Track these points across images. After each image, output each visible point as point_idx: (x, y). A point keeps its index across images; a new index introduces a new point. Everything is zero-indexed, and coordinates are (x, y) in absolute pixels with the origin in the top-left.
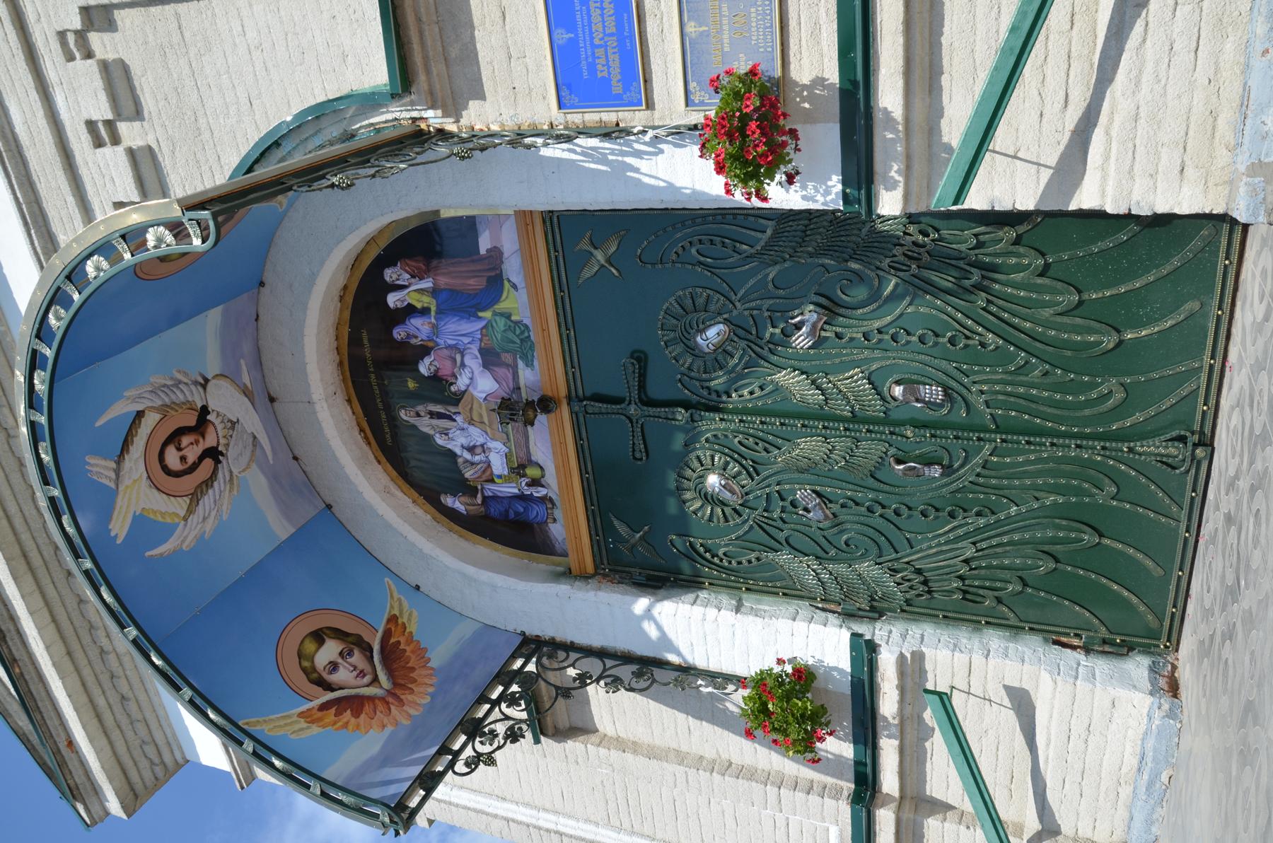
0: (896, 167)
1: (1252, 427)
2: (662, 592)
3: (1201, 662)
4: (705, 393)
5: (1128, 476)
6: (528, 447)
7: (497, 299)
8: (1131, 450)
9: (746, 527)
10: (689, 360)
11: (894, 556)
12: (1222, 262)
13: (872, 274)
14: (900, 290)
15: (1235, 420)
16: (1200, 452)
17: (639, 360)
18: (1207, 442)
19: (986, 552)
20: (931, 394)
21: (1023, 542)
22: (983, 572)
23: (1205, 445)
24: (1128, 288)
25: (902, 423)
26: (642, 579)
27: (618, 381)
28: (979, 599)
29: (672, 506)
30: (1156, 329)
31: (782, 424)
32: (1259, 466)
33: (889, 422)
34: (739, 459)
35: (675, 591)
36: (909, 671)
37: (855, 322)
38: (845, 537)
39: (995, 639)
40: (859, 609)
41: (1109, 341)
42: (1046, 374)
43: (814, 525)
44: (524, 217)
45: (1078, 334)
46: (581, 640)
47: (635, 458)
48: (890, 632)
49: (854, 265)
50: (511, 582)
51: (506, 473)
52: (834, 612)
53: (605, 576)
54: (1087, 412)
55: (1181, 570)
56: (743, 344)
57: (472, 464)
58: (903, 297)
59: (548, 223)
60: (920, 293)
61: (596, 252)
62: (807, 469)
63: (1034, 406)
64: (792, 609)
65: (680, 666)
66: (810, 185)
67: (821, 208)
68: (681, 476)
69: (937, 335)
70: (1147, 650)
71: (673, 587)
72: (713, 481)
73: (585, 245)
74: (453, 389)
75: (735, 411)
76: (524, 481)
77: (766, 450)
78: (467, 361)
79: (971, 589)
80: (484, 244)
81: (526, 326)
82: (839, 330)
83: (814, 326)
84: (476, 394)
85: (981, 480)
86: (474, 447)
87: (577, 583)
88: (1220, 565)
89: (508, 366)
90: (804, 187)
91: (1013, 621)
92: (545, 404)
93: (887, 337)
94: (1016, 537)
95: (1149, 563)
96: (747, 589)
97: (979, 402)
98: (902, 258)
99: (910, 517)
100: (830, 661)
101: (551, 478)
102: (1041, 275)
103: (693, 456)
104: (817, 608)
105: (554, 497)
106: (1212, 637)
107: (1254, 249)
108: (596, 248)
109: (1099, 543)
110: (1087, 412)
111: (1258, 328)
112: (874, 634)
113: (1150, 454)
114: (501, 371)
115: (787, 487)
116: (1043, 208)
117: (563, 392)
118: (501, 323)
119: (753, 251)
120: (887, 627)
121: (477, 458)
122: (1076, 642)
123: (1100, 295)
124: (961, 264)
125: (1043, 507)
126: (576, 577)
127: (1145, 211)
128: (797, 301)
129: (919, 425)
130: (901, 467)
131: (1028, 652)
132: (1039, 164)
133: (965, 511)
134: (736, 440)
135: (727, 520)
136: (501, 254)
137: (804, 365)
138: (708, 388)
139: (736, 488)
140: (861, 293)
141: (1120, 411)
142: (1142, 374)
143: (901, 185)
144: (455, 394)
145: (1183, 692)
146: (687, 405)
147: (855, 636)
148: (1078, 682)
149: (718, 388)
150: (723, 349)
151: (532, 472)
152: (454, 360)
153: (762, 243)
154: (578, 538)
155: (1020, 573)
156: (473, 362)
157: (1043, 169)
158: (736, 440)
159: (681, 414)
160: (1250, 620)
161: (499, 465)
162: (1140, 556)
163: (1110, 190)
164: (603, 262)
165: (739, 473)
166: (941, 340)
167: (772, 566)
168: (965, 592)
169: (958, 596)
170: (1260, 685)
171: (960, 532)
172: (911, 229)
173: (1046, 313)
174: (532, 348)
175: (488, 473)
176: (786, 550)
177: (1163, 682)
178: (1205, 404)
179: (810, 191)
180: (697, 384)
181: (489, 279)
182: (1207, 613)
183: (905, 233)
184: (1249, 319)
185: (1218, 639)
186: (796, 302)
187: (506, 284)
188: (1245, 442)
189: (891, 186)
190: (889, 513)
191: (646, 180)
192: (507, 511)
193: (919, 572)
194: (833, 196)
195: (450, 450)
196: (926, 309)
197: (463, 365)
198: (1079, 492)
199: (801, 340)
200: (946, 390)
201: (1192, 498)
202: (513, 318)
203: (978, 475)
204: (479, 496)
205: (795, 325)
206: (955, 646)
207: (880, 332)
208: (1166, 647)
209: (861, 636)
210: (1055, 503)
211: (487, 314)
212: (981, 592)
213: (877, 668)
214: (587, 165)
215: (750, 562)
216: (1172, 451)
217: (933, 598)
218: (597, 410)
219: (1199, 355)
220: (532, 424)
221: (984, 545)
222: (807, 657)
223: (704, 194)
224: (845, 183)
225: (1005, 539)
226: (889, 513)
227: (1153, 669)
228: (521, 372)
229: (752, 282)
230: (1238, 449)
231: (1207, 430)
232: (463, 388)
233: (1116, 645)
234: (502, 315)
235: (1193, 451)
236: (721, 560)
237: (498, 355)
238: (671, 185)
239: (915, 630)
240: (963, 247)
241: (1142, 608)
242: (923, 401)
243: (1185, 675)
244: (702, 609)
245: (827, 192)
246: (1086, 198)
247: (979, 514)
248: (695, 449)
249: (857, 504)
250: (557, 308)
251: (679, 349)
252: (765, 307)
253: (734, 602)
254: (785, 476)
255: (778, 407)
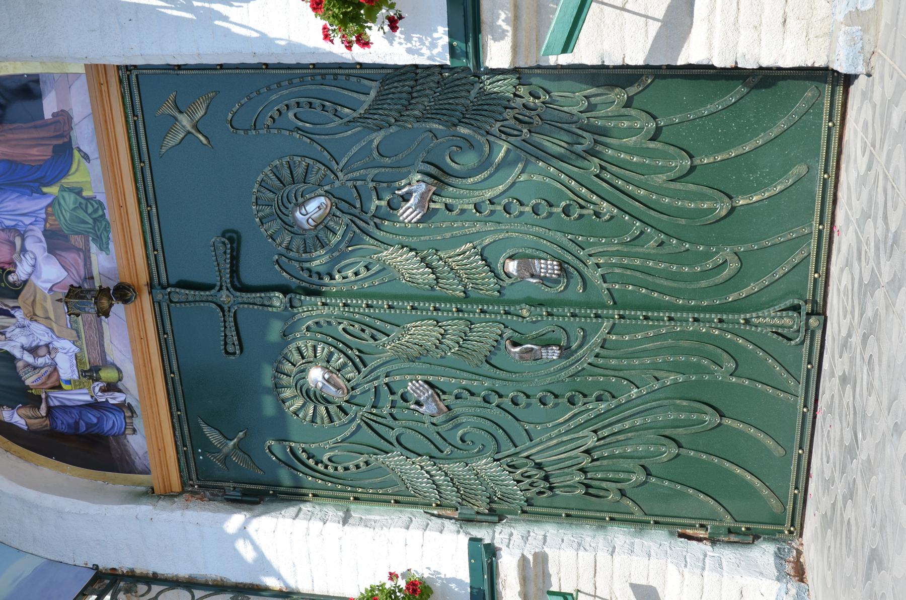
0: (503, 16)
1: (861, 279)
2: (259, 508)
3: (824, 537)
4: (305, 275)
5: (745, 349)
6: (102, 346)
7: (65, 171)
8: (747, 322)
9: (353, 427)
10: (288, 238)
11: (513, 450)
12: (825, 124)
13: (483, 140)
14: (512, 156)
15: (845, 280)
16: (813, 322)
17: (231, 240)
18: (819, 311)
19: (608, 440)
20: (547, 269)
21: (645, 428)
22: (605, 462)
23: (818, 314)
24: (738, 152)
25: (518, 302)
26: (237, 495)
27: (207, 266)
28: (602, 493)
29: (269, 406)
30: (767, 195)
31: (390, 307)
32: (869, 313)
33: (503, 300)
34: (344, 348)
35: (275, 505)
36: (532, 575)
37: (466, 192)
38: (460, 433)
39: (620, 535)
40: (478, 513)
41: (722, 209)
42: (661, 244)
43: (427, 419)
44: (96, 72)
45: (691, 201)
46: (166, 569)
47: (227, 353)
48: (511, 535)
49: (463, 130)
50: (81, 505)
51: (76, 377)
52: (450, 518)
53: (194, 493)
54: (703, 284)
55: (801, 448)
56: (346, 219)
57: (35, 368)
58: (515, 163)
59: (126, 83)
60: (533, 159)
61: (181, 117)
62: (416, 357)
63: (650, 279)
64: (405, 518)
65: (281, 591)
66: (415, 37)
67: (428, 63)
68: (279, 371)
69: (551, 205)
70: (772, 537)
71: (272, 501)
72: (316, 375)
73: (168, 109)
74: (11, 278)
75: (339, 294)
76: (98, 386)
77: (373, 337)
78: (29, 245)
79: (594, 483)
80: (50, 106)
81: (100, 204)
82: (449, 201)
83: (422, 196)
84: (40, 284)
85: (600, 361)
86: (38, 347)
87: (161, 503)
88: (838, 430)
89: (78, 250)
90: (408, 39)
91: (639, 516)
92: (124, 292)
93: (500, 208)
94: (638, 421)
95: (770, 442)
96: (356, 499)
97: (595, 276)
98: (512, 122)
99: (528, 405)
100: (448, 572)
101: (130, 382)
102: (653, 139)
103: (292, 347)
104: (433, 515)
105: (133, 404)
106: (834, 505)
107: (855, 108)
108: (181, 112)
109: (720, 424)
110: (703, 284)
111: (862, 180)
112: (493, 538)
113: (766, 325)
114: (70, 257)
115: (398, 378)
116: (653, 63)
117: (144, 278)
118: (70, 200)
119: (356, 115)
120: (507, 530)
121: (41, 361)
122: (701, 533)
123: (711, 160)
124: (573, 128)
125: (663, 387)
126: (159, 496)
127: (751, 65)
128: (405, 170)
129: (533, 303)
130: (517, 349)
131: (654, 547)
132: (647, 17)
133: (585, 396)
134: (341, 327)
135: (331, 421)
136: (70, 119)
137: (412, 241)
138: (309, 270)
139: (341, 382)
140: (469, 159)
141: (733, 282)
142: (755, 241)
143: (510, 34)
144: (13, 284)
145: (809, 575)
146: (285, 290)
147: (473, 540)
148: (706, 573)
149: (320, 269)
150: (323, 225)
151: (107, 375)
152: (13, 244)
153: (366, 106)
154: (161, 450)
155: (643, 462)
156: (36, 246)
157: (651, 21)
158: (341, 327)
159: (278, 300)
160: (869, 468)
161: (67, 369)
162: (761, 436)
163: (716, 43)
164: (189, 128)
165: (344, 365)
166: (555, 210)
167: (381, 470)
168: (587, 486)
169: (581, 491)
170: (882, 529)
171: (581, 419)
172: (522, 90)
173: (660, 179)
174: (107, 228)
175: (54, 378)
176: (398, 450)
177: (789, 568)
178: (816, 272)
179: (415, 43)
180: (297, 265)
181: (57, 150)
182: (828, 484)
183: (515, 95)
184: (853, 174)
185: (840, 504)
186: (402, 169)
187: (76, 154)
188: (856, 295)
189: (499, 36)
190: (507, 402)
191: (236, 30)
192: (77, 423)
193: (539, 466)
194: (439, 49)
195: (7, 352)
196: (538, 177)
197: (24, 250)
198: (699, 369)
199: (409, 213)
200: (562, 263)
201: (808, 371)
202: (85, 194)
203: (597, 356)
204: (43, 406)
205: (402, 196)
206: (579, 544)
207: (492, 202)
208: (791, 532)
209: (480, 540)
210: (675, 383)
211: (53, 190)
212: (604, 485)
213: (498, 574)
214: (169, 12)
215: (358, 467)
216: (787, 321)
217: (555, 495)
218: (183, 298)
219: (808, 222)
220: (107, 315)
221: (606, 432)
222: (422, 570)
223: (300, 46)
224: (450, 35)
225: (627, 425)
226: (507, 402)
227: (779, 556)
228: (94, 258)
229: (355, 149)
230: (849, 308)
231: (819, 299)
232: (23, 277)
233: (744, 535)
234: (71, 190)
235: (807, 320)
236: (326, 467)
237: (66, 237)
238: (263, 36)
239: (538, 531)
240: (574, 110)
241: (766, 492)
242: (539, 277)
243: (810, 558)
244: (305, 522)
245: (433, 45)
246: (693, 53)
247: (599, 399)
248: (295, 339)
249: (472, 394)
250: (136, 181)
251: (275, 225)
252: (370, 177)
253: (341, 514)
254: (395, 366)
255: (385, 289)
